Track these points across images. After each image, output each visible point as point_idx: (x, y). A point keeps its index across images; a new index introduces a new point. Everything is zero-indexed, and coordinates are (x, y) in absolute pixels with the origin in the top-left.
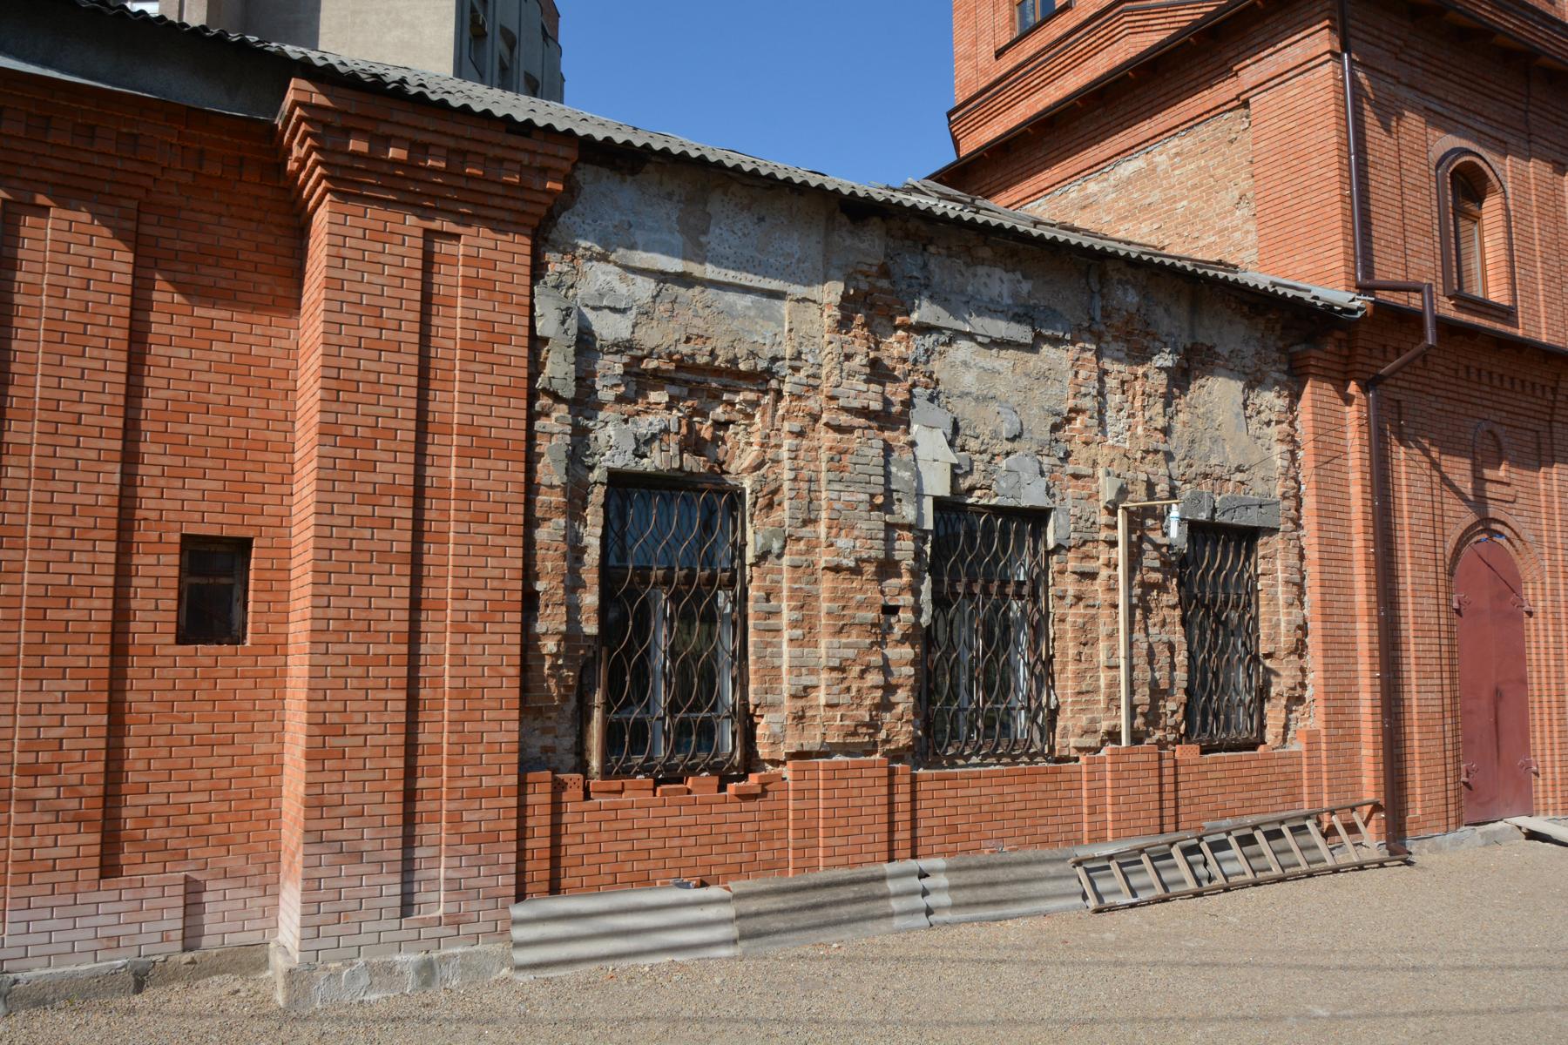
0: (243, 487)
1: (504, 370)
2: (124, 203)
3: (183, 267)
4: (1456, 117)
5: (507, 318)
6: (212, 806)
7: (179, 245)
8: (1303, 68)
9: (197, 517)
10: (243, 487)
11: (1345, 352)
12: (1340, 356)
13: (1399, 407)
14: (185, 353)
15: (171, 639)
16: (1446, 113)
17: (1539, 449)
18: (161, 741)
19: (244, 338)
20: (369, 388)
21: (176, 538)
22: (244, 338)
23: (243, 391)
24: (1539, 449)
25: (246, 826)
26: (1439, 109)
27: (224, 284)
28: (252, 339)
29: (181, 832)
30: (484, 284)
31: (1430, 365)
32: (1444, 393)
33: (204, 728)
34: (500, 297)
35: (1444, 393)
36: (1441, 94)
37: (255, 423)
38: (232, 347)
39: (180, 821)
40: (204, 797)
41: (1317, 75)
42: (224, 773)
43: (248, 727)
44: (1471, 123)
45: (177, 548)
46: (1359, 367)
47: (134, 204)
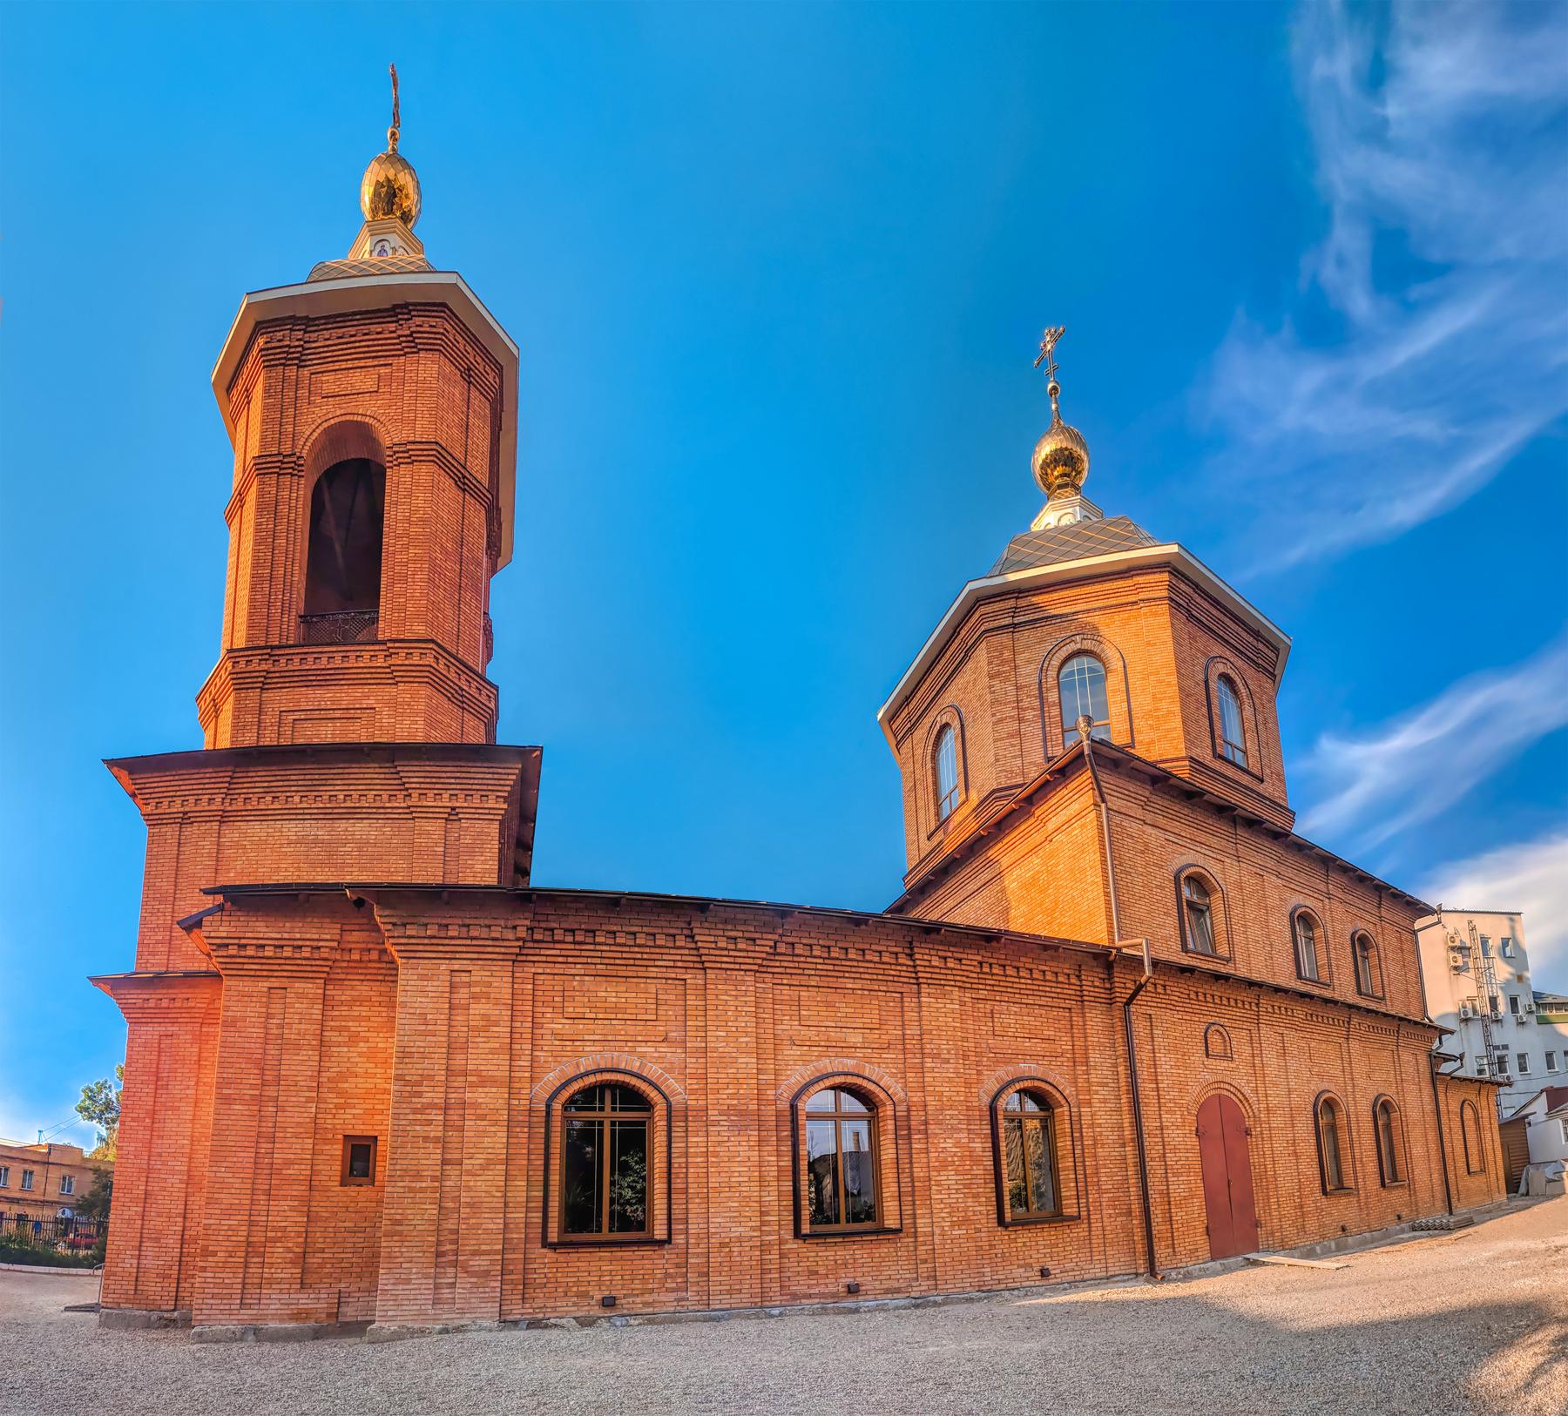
0: (373, 1112)
1: (496, 1040)
2: (318, 981)
3: (346, 1008)
4: (1188, 845)
5: (497, 1012)
6: (354, 1260)
7: (343, 998)
8: (1079, 815)
9: (351, 1127)
10: (373, 1112)
11: (1108, 986)
12: (1106, 989)
13: (1151, 1018)
14: (346, 1049)
15: (337, 1183)
16: (1180, 842)
17: (1251, 1040)
18: (331, 1230)
19: (374, 1040)
20: (420, 1055)
21: (340, 1137)
22: (374, 1040)
23: (373, 1065)
24: (1251, 1040)
25: (371, 1269)
26: (1176, 841)
27: (364, 1014)
28: (378, 1040)
29: (339, 1271)
30: (484, 995)
31: (1168, 992)
32: (1182, 1009)
33: (351, 1225)
34: (494, 1001)
35: (1182, 1009)
36: (1176, 831)
37: (379, 1081)
38: (368, 1045)
39: (338, 1265)
40: (350, 1255)
41: (850, 1062)
42: (360, 1245)
43: (373, 1224)
44: (1199, 849)
45: (341, 1142)
46: (1118, 995)
47: (322, 981)
